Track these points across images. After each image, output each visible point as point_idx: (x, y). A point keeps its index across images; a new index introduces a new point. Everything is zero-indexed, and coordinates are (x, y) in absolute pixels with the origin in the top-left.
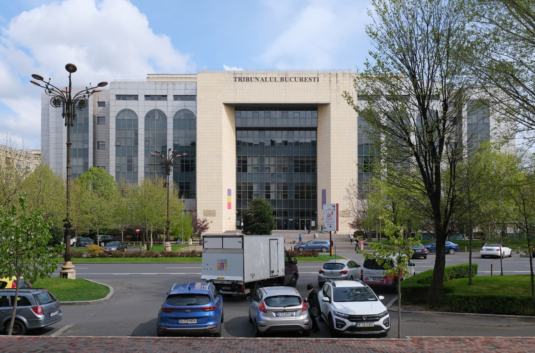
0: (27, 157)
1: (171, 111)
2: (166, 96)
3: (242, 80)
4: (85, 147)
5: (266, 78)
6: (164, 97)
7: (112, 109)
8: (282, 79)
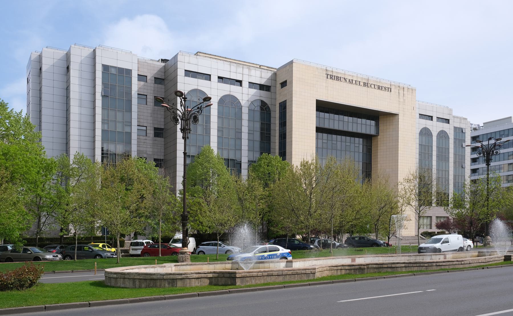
1: (247, 99)
2: (210, 80)
4: (127, 129)
6: (240, 82)
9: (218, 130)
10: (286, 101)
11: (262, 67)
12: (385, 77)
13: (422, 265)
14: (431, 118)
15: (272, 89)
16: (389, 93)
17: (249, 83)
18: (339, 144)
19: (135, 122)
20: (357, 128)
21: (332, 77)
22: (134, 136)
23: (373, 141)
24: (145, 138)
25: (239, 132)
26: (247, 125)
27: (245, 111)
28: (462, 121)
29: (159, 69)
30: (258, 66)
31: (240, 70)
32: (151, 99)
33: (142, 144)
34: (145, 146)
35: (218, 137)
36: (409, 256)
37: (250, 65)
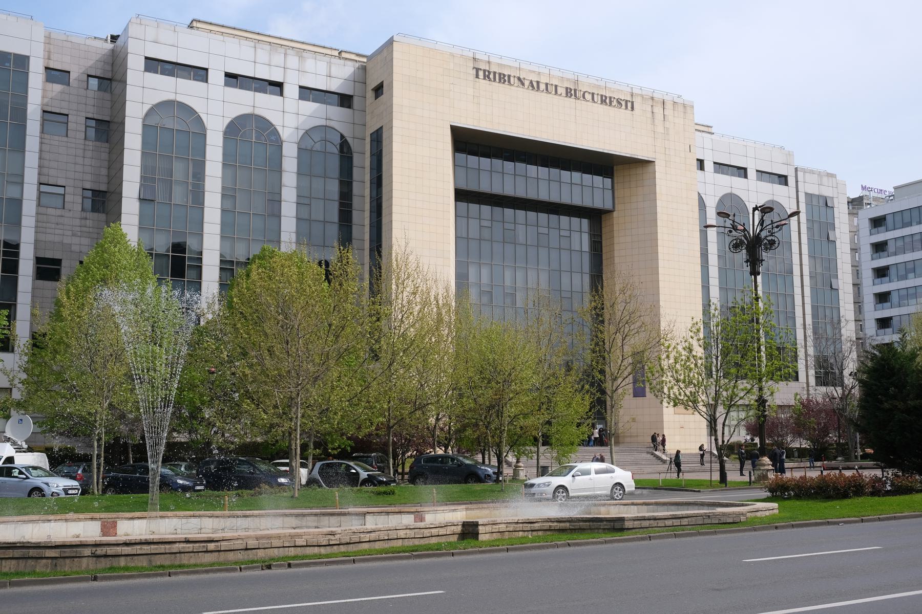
0: (166, 484)
1: (295, 125)
2: (207, 82)
3: (491, 76)
5: (538, 83)
7: (132, 93)
8: (569, 92)
9: (223, 196)
10: (381, 128)
11: (344, 55)
12: (597, 71)
13: (32, 552)
14: (742, 172)
15: (356, 101)
16: (629, 112)
17: (301, 87)
18: (521, 229)
19: (31, 176)
20: (551, 190)
21: (488, 74)
22: (29, 208)
23: (603, 225)
24: (59, 212)
25: (275, 201)
26: (295, 184)
27: (290, 153)
28: (825, 179)
29: (98, 57)
30: (336, 53)
31: (278, 58)
32: (77, 123)
33: (53, 226)
34: (61, 232)
35: (224, 211)
36: (297, 515)
37: (301, 48)
